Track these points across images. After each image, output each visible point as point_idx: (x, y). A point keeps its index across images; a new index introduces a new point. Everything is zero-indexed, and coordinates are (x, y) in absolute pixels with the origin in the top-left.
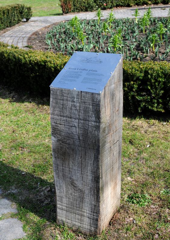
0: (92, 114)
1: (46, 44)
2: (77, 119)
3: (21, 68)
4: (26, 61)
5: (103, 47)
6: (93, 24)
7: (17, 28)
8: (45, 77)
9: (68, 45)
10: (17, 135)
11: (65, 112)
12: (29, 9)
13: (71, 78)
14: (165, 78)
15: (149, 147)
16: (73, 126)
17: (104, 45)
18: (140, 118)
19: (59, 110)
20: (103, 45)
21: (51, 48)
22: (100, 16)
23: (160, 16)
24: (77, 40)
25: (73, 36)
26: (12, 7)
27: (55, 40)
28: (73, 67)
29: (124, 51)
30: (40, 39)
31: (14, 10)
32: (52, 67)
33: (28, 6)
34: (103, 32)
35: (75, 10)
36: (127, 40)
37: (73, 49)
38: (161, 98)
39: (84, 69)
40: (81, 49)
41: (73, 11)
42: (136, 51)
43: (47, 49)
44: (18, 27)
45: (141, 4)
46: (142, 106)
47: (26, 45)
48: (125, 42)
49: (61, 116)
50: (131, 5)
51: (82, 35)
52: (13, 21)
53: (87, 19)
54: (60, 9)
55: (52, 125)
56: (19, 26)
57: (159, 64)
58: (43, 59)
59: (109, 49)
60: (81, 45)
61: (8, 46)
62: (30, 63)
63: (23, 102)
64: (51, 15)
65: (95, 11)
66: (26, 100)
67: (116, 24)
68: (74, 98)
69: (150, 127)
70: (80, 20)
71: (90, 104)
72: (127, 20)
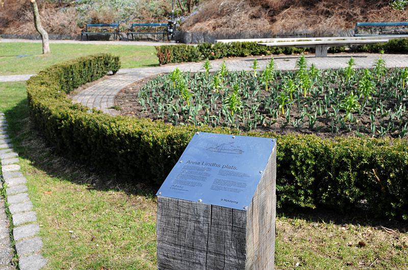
0: (231, 245)
1: (139, 104)
2: (205, 251)
3: (106, 140)
4: (113, 132)
5: (215, 108)
6: (199, 78)
7: (100, 83)
8: (139, 155)
9: (168, 106)
10: (97, 245)
11: (182, 238)
12: (117, 59)
13: (192, 181)
14: (315, 159)
15: (300, 265)
16: (196, 263)
17: (217, 106)
18: (279, 217)
19: (172, 234)
20: (215, 105)
21: (145, 110)
22: (209, 68)
23: (284, 69)
24: (180, 100)
25: (175, 93)
26: (95, 57)
27: (151, 98)
28: (195, 160)
29: (245, 115)
30: (131, 97)
31: (98, 61)
32: (150, 141)
33: (116, 56)
34: (214, 87)
35: (176, 60)
36: (246, 99)
37: (175, 111)
38: (310, 187)
39: (214, 165)
40: (186, 112)
41: (173, 62)
42: (261, 114)
43: (140, 111)
44: (102, 82)
45: (258, 54)
46: (282, 199)
47: (112, 106)
48: (245, 103)
49: (175, 245)
50: (245, 55)
51: (186, 92)
52: (95, 74)
53: (191, 71)
54: (156, 58)
55: (159, 259)
56: (103, 80)
57: (304, 139)
58: (137, 130)
59: (224, 111)
60: (186, 106)
61: (87, 110)
62: (119, 135)
63: (107, 190)
64: (144, 66)
65: (200, 61)
66: (112, 186)
67: (230, 78)
68: (200, 216)
69: (295, 231)
70: (182, 73)
71: (229, 227)
72: (243, 73)
